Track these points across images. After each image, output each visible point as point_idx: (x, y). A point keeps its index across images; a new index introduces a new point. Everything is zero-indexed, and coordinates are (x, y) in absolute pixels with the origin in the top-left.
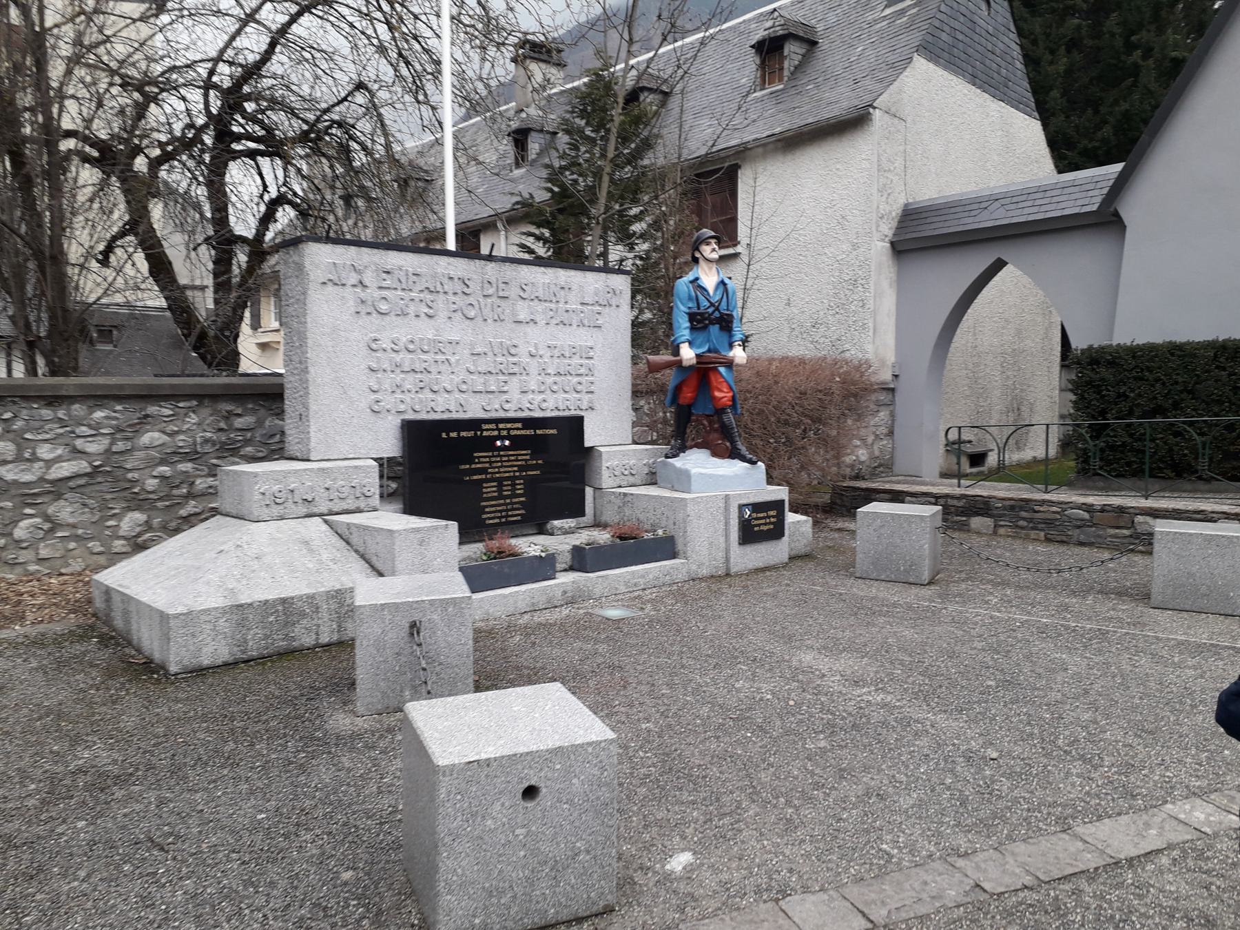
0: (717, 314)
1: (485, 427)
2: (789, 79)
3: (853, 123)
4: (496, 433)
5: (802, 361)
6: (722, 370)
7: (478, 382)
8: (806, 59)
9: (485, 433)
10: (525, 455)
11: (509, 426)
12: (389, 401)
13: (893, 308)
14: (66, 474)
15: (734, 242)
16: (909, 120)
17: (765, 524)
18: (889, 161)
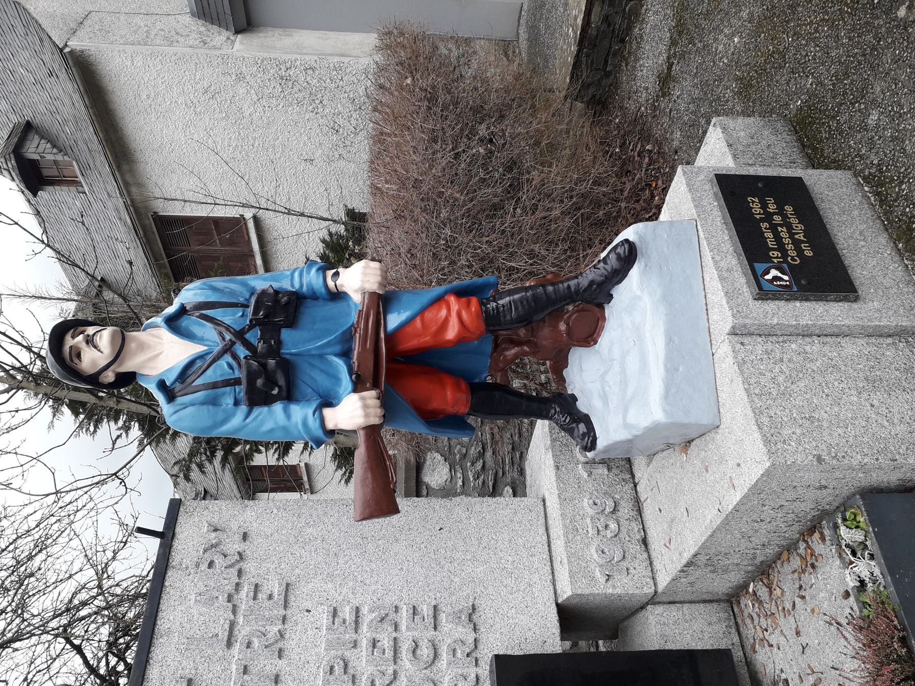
0: (253, 336)
2: (66, 154)
3: (86, 74)
5: (379, 138)
6: (394, 320)
8: (44, 135)
13: (317, 34)
16: (89, 8)
17: (789, 227)
18: (135, 32)
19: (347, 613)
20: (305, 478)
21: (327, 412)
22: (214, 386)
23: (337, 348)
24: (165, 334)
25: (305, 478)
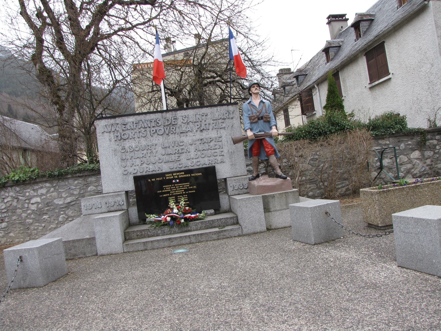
4: (172, 177)
7: (167, 158)
9: (167, 178)
10: (187, 185)
11: (178, 174)
14: (69, 201)
19: (220, 139)
20: (377, 83)
21: (249, 130)
22: (252, 110)
23: (261, 130)
24: (259, 101)
25: (377, 83)
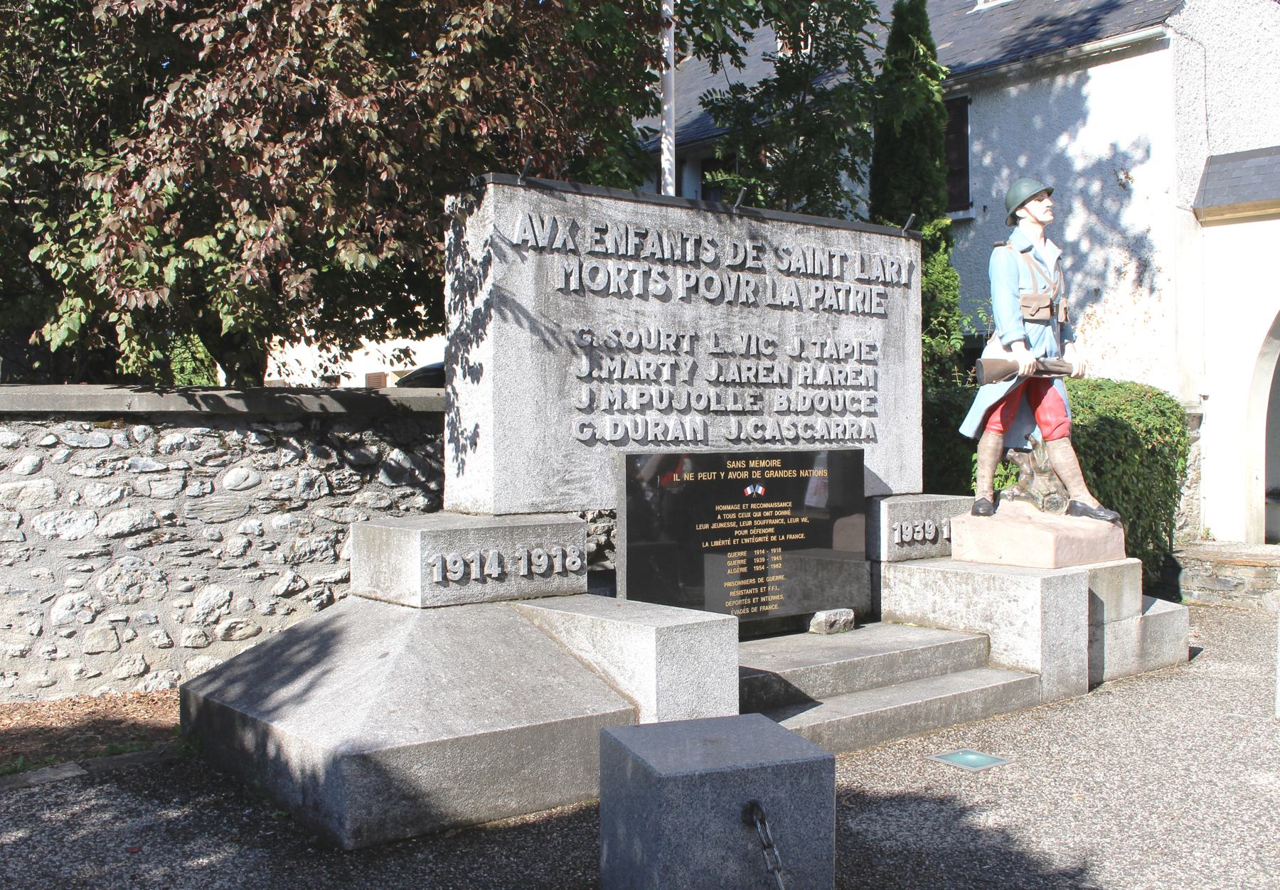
1: (730, 465)
4: (745, 475)
9: (731, 475)
11: (763, 464)
12: (604, 425)
15: (967, 205)
